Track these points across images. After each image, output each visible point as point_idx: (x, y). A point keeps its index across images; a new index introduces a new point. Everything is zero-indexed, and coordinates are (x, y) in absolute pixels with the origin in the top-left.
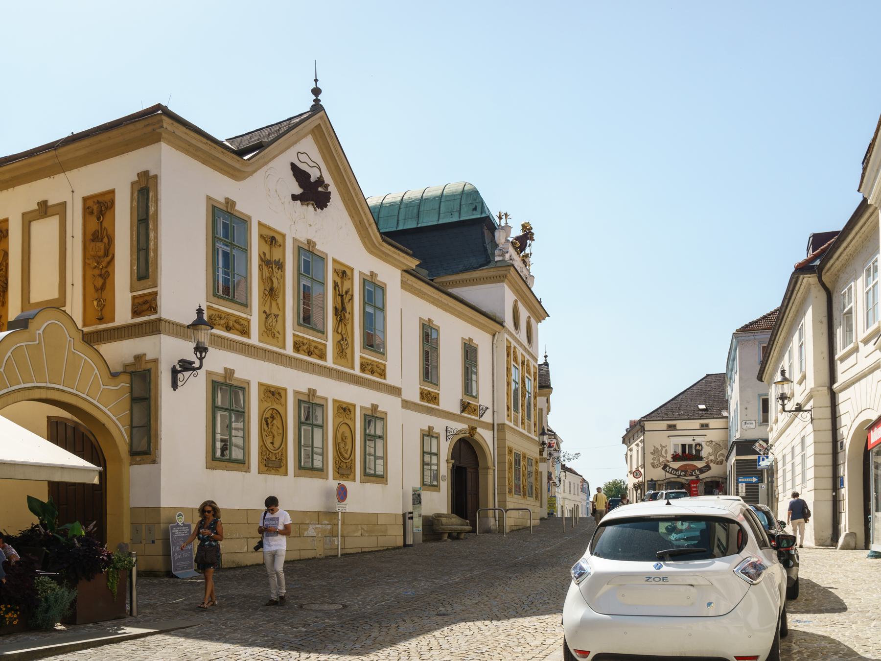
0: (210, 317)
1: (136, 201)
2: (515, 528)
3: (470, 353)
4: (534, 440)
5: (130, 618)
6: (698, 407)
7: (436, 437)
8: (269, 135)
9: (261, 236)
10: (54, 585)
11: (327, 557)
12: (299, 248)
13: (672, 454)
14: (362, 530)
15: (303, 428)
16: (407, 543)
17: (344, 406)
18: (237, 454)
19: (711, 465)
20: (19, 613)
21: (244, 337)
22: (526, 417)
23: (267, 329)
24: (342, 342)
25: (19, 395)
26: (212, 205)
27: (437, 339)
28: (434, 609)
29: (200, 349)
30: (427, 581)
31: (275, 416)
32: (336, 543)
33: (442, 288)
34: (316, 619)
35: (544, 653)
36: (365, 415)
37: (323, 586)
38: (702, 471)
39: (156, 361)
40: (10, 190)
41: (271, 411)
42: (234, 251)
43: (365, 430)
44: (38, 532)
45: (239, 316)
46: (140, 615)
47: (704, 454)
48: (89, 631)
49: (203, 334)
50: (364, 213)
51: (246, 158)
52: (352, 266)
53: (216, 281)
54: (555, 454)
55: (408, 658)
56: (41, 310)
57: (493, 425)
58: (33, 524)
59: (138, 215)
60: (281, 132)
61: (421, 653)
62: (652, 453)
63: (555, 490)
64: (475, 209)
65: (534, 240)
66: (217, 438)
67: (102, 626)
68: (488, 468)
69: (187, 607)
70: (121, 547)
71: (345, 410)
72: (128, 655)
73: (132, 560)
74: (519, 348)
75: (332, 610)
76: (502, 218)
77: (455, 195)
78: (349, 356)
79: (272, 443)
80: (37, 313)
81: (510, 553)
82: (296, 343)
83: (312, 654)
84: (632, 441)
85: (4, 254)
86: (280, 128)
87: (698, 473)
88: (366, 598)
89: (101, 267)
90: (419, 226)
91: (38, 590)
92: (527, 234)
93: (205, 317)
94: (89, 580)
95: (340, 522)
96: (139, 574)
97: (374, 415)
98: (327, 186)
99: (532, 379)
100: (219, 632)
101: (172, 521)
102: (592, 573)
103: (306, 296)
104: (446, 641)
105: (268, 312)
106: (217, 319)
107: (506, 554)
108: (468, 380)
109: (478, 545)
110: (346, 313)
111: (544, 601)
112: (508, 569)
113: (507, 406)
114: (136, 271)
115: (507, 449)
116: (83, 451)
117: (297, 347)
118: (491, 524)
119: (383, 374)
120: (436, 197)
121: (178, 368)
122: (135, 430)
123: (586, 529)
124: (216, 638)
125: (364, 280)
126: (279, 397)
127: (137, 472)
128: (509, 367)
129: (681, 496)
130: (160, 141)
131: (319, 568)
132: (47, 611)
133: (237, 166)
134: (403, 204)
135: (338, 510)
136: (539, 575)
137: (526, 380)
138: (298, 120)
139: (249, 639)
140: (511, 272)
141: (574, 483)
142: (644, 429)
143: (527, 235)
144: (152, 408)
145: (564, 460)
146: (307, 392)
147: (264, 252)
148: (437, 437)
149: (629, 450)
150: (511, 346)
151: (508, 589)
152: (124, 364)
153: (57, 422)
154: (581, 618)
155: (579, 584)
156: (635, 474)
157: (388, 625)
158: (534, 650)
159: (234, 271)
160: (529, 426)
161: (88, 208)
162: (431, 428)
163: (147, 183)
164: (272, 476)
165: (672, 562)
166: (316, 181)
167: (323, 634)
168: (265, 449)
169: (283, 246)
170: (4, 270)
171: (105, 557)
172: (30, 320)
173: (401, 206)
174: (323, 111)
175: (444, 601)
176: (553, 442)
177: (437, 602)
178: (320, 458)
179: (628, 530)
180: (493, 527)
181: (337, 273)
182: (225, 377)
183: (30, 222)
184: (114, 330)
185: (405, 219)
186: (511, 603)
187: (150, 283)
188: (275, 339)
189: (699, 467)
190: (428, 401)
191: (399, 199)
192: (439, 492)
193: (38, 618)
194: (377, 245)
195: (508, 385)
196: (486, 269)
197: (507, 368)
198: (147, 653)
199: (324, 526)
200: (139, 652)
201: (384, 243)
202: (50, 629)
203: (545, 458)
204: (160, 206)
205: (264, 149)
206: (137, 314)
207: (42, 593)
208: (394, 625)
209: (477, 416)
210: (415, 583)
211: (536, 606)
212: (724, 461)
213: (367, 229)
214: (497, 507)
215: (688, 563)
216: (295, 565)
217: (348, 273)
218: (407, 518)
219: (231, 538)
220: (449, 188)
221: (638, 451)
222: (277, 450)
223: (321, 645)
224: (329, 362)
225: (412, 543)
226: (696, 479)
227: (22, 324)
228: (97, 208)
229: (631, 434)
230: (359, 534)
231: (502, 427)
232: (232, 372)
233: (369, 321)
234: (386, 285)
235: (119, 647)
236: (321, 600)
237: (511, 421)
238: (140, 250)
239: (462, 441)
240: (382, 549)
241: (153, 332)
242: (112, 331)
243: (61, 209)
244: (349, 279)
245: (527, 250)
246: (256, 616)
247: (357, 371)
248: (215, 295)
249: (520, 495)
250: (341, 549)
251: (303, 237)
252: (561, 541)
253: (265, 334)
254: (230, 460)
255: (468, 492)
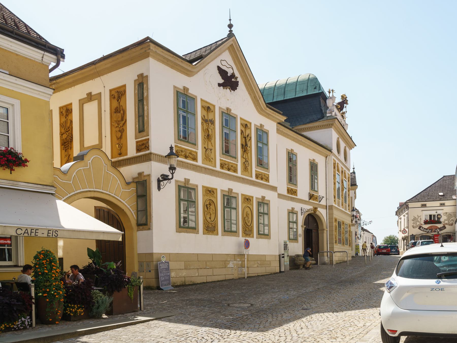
0: (177, 151)
1: (137, 90)
2: (338, 262)
3: (313, 167)
4: (348, 214)
5: (140, 311)
6: (439, 194)
7: (296, 213)
8: (206, 51)
9: (203, 107)
10: (101, 294)
11: (239, 278)
12: (223, 112)
13: (424, 220)
14: (258, 264)
15: (226, 209)
16: (281, 271)
17: (247, 198)
18: (192, 224)
19: (446, 226)
20: (84, 309)
21: (195, 161)
22: (344, 202)
23: (206, 157)
24: (246, 163)
25: (80, 195)
26: (177, 91)
27: (296, 161)
28: (301, 306)
29: (172, 168)
30: (294, 291)
31: (211, 204)
32: (244, 271)
33: (299, 132)
34: (237, 312)
35: (366, 331)
36: (258, 202)
37: (240, 294)
38: (441, 229)
39: (149, 176)
40: (73, 88)
41: (209, 200)
42: (188, 115)
43: (258, 210)
44: (92, 267)
45: (192, 150)
46: (145, 310)
47: (442, 220)
48: (119, 318)
49: (173, 160)
50: (257, 92)
51: (194, 64)
52: (250, 121)
53: (179, 131)
54: (359, 222)
55: (290, 333)
56: (90, 150)
57: (326, 206)
58: (89, 263)
59: (138, 98)
60: (212, 49)
61: (297, 331)
62: (413, 220)
63: (358, 241)
64: (315, 88)
65: (348, 104)
66: (181, 216)
67: (126, 316)
68: (324, 230)
69: (169, 306)
70: (134, 274)
71: (247, 199)
72: (140, 331)
73: (140, 281)
74: (340, 164)
75: (245, 307)
76: (330, 92)
77: (304, 81)
78: (249, 170)
79: (210, 218)
80: (88, 152)
81: (338, 275)
82: (222, 164)
83: (237, 331)
84: (401, 213)
85: (71, 122)
86: (211, 47)
87: (438, 230)
88: (263, 300)
89: (120, 126)
90: (285, 99)
91: (93, 297)
92: (344, 101)
93: (174, 151)
94: (119, 292)
95: (246, 259)
96: (145, 288)
97: (263, 202)
98: (236, 78)
99: (347, 181)
100: (187, 319)
101: (159, 260)
102: (398, 286)
103: (226, 139)
104: (310, 324)
105: (207, 148)
106: (180, 152)
107: (336, 276)
108: (312, 182)
109: (319, 271)
110: (248, 147)
111: (361, 301)
112: (338, 284)
113: (334, 196)
114: (138, 128)
115: (334, 219)
116: (113, 224)
117: (222, 166)
118: (326, 260)
119: (267, 180)
120: (294, 83)
121: (161, 179)
122: (139, 213)
123: (377, 262)
124: (186, 322)
125: (257, 129)
126: (213, 193)
127: (141, 235)
128: (335, 174)
129: (430, 243)
130: (149, 57)
131: (236, 285)
132: (98, 308)
133: (189, 68)
134: (276, 87)
135: (245, 253)
136: (355, 287)
137: (344, 181)
138: (221, 42)
139: (203, 323)
140: (336, 122)
141: (368, 238)
142: (408, 207)
143: (344, 102)
144: (148, 201)
145: (363, 225)
146: (228, 190)
147: (204, 115)
148: (296, 214)
149: (399, 219)
150: (336, 163)
151: (340, 295)
152: (133, 178)
153: (99, 209)
154: (393, 311)
155: (390, 292)
156: (403, 232)
157: (277, 315)
158: (360, 329)
159: (188, 126)
160: (346, 206)
161: (112, 95)
162: (293, 209)
163: (143, 80)
164: (210, 236)
165: (446, 280)
166: (231, 75)
167: (242, 320)
168: (206, 221)
169: (214, 112)
170: (71, 130)
171: (126, 280)
172: (85, 156)
173: (275, 88)
174: (234, 37)
175: (305, 301)
176: (358, 215)
177: (302, 302)
178: (235, 226)
179: (419, 261)
180: (327, 262)
181: (243, 125)
182: (185, 183)
183: (83, 104)
184: (127, 160)
185: (277, 96)
186: (342, 302)
187: (145, 134)
188: (211, 162)
189: (440, 227)
190: (292, 194)
191: (274, 84)
192: (298, 243)
193: (94, 312)
194: (264, 109)
195: (334, 185)
196: (321, 121)
197: (334, 175)
198: (150, 330)
199: (237, 262)
200: (146, 330)
201: (267, 108)
202: (100, 317)
203: (353, 224)
204: (150, 92)
205: (204, 59)
206: (139, 151)
207: (95, 298)
208: (280, 315)
209: (318, 202)
210: (288, 292)
211: (357, 304)
212: (454, 224)
213: (258, 101)
214: (329, 250)
215: (455, 280)
216: (223, 283)
217: (249, 125)
218: (281, 257)
219: (190, 269)
220: (301, 77)
221: (404, 219)
222: (212, 222)
223: (241, 326)
224: (239, 174)
225: (284, 270)
226: (437, 234)
227: (80, 158)
228: (117, 95)
229: (400, 210)
230: (256, 266)
231: (331, 207)
232: (189, 180)
233: (260, 151)
234: (268, 131)
235: (135, 327)
236: (239, 301)
237: (336, 204)
238: (140, 116)
239: (309, 215)
240: (268, 274)
241: (147, 160)
242: (126, 160)
243: (99, 96)
244: (249, 128)
245: (344, 110)
246: (206, 310)
247: (254, 178)
248: (179, 139)
249: (341, 244)
250: (247, 274)
251: (224, 107)
252: (365, 269)
253: (205, 159)
254: (188, 228)
255: (313, 243)
